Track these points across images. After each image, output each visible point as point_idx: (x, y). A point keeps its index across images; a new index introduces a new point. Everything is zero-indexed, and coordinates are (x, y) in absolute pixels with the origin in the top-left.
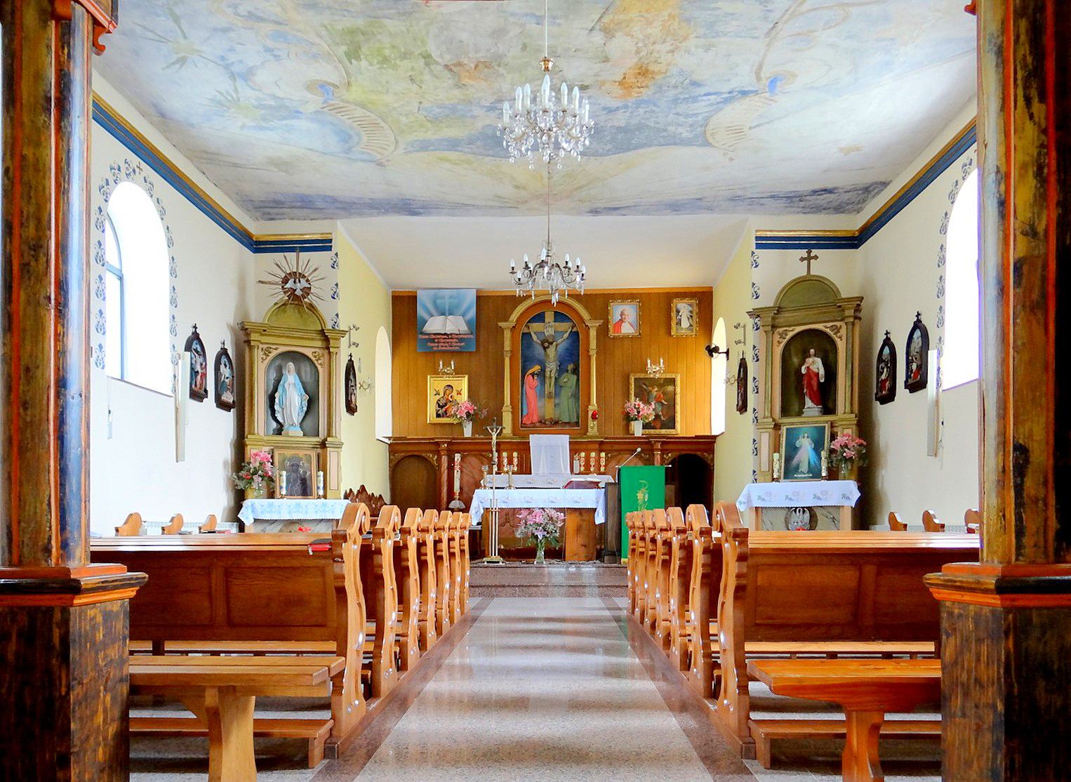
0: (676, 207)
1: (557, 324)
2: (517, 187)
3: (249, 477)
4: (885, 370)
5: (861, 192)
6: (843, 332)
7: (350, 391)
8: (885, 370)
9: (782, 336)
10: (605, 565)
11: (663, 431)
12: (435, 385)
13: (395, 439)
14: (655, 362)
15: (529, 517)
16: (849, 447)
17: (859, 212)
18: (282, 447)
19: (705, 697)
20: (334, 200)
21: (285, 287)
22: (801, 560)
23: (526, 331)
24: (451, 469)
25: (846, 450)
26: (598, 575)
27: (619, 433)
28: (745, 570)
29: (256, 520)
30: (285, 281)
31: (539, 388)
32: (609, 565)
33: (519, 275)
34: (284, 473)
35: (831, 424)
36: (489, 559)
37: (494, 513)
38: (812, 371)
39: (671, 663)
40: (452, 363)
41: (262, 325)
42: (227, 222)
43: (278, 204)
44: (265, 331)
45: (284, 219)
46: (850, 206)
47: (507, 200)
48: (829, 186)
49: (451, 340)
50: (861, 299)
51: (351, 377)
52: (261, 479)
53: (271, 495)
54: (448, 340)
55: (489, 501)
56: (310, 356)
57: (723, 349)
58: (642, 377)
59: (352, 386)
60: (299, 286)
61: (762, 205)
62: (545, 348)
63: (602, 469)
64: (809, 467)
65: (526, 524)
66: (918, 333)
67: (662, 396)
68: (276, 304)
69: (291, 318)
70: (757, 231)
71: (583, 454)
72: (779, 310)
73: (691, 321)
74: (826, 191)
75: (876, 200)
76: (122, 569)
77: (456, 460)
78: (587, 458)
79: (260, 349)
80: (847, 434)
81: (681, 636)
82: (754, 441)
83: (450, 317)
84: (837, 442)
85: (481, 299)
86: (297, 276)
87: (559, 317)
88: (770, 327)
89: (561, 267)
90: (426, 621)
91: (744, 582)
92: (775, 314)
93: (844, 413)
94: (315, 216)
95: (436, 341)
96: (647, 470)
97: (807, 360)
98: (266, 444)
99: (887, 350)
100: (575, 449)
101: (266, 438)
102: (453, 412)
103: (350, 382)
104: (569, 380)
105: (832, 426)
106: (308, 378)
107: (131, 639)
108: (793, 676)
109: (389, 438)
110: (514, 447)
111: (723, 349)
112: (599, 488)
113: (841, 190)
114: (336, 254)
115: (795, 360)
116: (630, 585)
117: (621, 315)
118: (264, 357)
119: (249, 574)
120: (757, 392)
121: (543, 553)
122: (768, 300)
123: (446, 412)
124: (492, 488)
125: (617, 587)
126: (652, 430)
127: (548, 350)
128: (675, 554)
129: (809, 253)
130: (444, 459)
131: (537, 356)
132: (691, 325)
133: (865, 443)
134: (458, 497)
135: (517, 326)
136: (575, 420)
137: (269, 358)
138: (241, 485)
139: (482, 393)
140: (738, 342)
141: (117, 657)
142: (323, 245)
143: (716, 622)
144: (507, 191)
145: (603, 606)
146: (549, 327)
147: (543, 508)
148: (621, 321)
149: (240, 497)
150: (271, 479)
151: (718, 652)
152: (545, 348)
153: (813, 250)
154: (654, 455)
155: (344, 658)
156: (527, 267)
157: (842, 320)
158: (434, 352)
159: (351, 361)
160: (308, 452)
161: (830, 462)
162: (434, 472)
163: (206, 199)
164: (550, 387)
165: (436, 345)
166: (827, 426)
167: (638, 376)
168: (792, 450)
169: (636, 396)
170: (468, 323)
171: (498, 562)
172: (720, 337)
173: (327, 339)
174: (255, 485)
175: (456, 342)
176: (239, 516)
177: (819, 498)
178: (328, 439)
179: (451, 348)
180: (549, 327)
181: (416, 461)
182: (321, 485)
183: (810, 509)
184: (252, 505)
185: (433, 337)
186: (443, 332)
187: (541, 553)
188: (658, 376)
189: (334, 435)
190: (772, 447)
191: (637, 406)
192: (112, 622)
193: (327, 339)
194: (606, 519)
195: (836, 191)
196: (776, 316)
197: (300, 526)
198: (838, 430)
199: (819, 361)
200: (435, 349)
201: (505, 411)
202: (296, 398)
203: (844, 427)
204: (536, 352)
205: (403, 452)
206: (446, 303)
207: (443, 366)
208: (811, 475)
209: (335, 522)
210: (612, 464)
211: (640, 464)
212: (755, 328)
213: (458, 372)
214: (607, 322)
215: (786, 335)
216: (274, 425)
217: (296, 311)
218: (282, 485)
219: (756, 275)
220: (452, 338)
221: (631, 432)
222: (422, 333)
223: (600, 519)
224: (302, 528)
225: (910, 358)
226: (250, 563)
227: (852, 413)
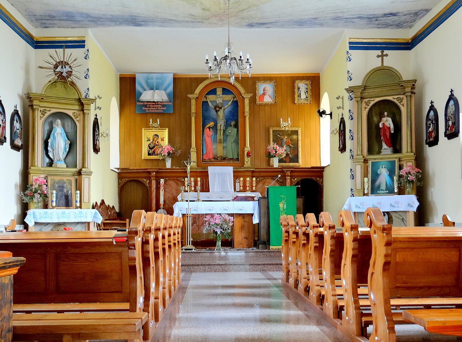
0: (301, 23)
1: (224, 96)
2: (204, 9)
3: (32, 194)
4: (431, 125)
5: (413, 15)
6: (404, 101)
7: (96, 138)
8: (431, 125)
9: (367, 104)
10: (260, 251)
11: (291, 164)
12: (147, 135)
13: (122, 169)
14: (285, 120)
15: (212, 220)
16: (411, 174)
17: (411, 28)
18: (53, 175)
19: (357, 336)
20: (88, 16)
21: (56, 71)
22: (424, 245)
23: (205, 100)
24: (158, 189)
25: (409, 175)
26: (247, 257)
27: (264, 165)
28: (390, 252)
29: (36, 223)
30: (56, 67)
31: (213, 136)
32: (263, 250)
33: (210, 65)
34: (54, 192)
35: (399, 159)
36: (186, 248)
37: (189, 217)
38: (386, 126)
39: (326, 315)
40: (158, 120)
41: (41, 95)
42: (19, 28)
43: (51, 17)
44: (42, 99)
45: (54, 27)
46: (406, 24)
47: (197, 17)
48: (394, 11)
49: (158, 106)
50: (415, 81)
51: (97, 129)
52: (39, 196)
53: (46, 206)
54: (155, 106)
55: (186, 209)
56: (71, 115)
57: (328, 112)
58: (277, 129)
59: (97, 135)
60: (65, 70)
61: (353, 22)
62: (217, 111)
63: (254, 188)
64: (386, 186)
65: (209, 225)
66: (452, 102)
67: (290, 141)
68: (50, 81)
69: (60, 91)
70: (350, 39)
71: (242, 179)
72: (365, 88)
73: (307, 95)
74: (392, 14)
75: (422, 19)
76: (10, 254)
77: (161, 183)
78: (245, 182)
79: (39, 111)
80: (409, 166)
81: (333, 296)
82: (351, 170)
83: (156, 91)
84: (404, 170)
85: (176, 80)
86: (63, 64)
87: (226, 91)
88: (360, 98)
89: (237, 60)
90: (165, 288)
91: (389, 259)
92: (362, 90)
93: (407, 152)
94: (75, 26)
95: (148, 106)
96: (283, 188)
97: (383, 119)
98: (42, 173)
99: (432, 113)
100: (237, 175)
101: (42, 169)
102: (159, 152)
103: (96, 132)
104: (232, 131)
105: (400, 161)
106: (69, 129)
107: (14, 303)
108: (438, 320)
109: (118, 169)
110: (198, 174)
111: (328, 112)
112: (254, 200)
113: (401, 14)
114: (88, 50)
115: (375, 119)
116: (284, 263)
117: (264, 90)
118: (42, 116)
119: (72, 258)
120: (352, 139)
121: (220, 243)
122: (358, 81)
123: (154, 152)
124: (187, 201)
125: (270, 264)
126: (284, 163)
127: (219, 113)
128: (326, 242)
129: (382, 52)
130: (154, 182)
131: (212, 116)
132: (307, 97)
133: (421, 171)
134: (162, 207)
135: (199, 97)
136: (236, 157)
137: (45, 117)
138: (26, 200)
139: (177, 139)
140: (339, 108)
141: (7, 315)
142: (80, 44)
143: (367, 286)
144: (197, 11)
145: (264, 277)
146: (219, 98)
147: (220, 214)
148: (264, 94)
149: (25, 208)
150: (46, 196)
151: (370, 306)
152: (217, 111)
153: (384, 51)
154: (286, 179)
155: (147, 313)
156: (216, 59)
157: (404, 94)
158: (147, 113)
159: (96, 119)
160: (70, 178)
161: (400, 183)
162: (147, 191)
163: (6, 13)
164: (220, 136)
165: (148, 108)
166: (397, 160)
167: (275, 129)
168: (375, 176)
169: (274, 141)
170: (168, 95)
171: (192, 249)
172: (325, 104)
173: (82, 105)
174: (35, 200)
175: (160, 107)
176: (25, 220)
177: (394, 206)
178: (83, 169)
179: (157, 111)
180: (219, 98)
181: (136, 184)
182: (78, 200)
183: (388, 213)
184: (33, 213)
185: (146, 104)
186: (152, 101)
187: (219, 243)
188: (287, 129)
189: (86, 167)
190: (363, 174)
191: (275, 148)
192: (4, 291)
193: (82, 105)
194: (260, 220)
195: (398, 15)
196: (363, 91)
197: (65, 227)
198: (404, 163)
199: (390, 120)
200: (147, 111)
201: (192, 152)
202: (62, 143)
203: (408, 161)
204: (212, 113)
205: (127, 178)
206: (154, 82)
207: (152, 123)
208: (388, 191)
209: (87, 224)
210: (260, 185)
211: (277, 185)
212: (350, 99)
213: (162, 126)
214: (255, 95)
215: (370, 103)
216: (47, 160)
217: (63, 86)
218: (77, 200)
219: (350, 66)
220: (158, 105)
221: (271, 165)
222: (138, 101)
223: (256, 220)
224: (66, 228)
225: (447, 118)
226: (73, 250)
227: (412, 152)
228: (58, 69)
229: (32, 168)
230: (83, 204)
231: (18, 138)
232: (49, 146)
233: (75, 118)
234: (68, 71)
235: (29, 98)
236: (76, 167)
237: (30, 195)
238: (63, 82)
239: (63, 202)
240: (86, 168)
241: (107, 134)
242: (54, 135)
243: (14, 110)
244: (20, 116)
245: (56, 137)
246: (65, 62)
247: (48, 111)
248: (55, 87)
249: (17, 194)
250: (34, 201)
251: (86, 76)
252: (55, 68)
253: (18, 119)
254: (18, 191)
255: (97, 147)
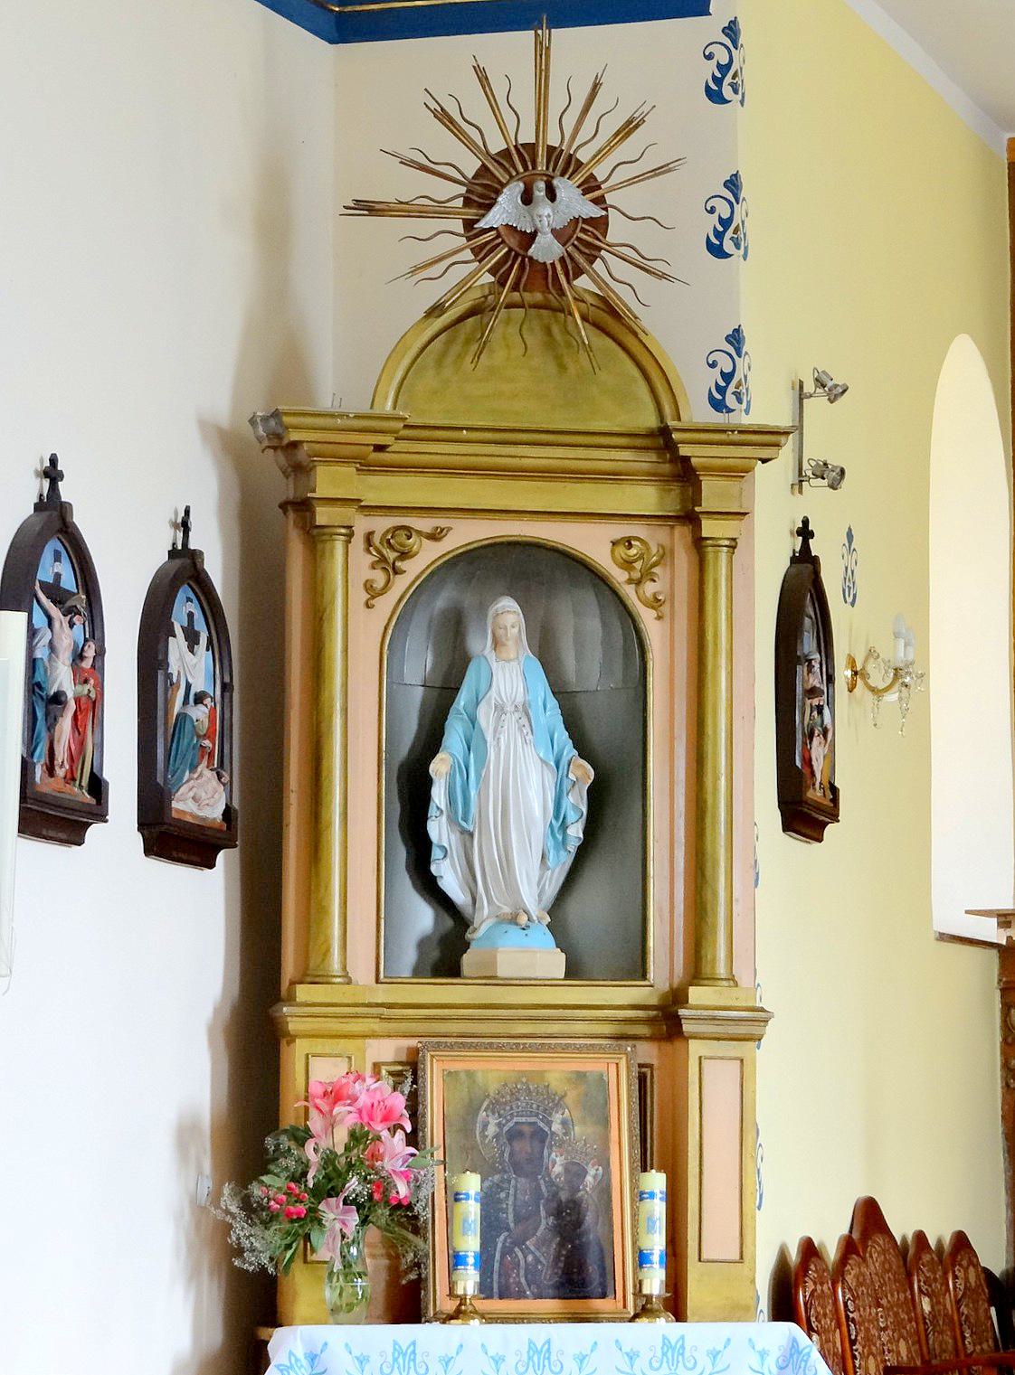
7: (802, 719)
21: (482, 224)
30: (482, 194)
34: (472, 1183)
41: (368, 422)
44: (380, 448)
52: (354, 1219)
60: (547, 216)
68: (436, 310)
79: (358, 541)
101: (383, 994)
114: (732, 30)
118: (379, 578)
137: (401, 584)
138: (261, 1246)
150: (408, 1219)
159: (805, 562)
160: (592, 1065)
173: (685, 475)
174: (326, 1248)
178: (692, 990)
182: (656, 1242)
184: (312, 1358)
189: (721, 970)
216: (423, 917)
217: (534, 339)
228: (495, 209)
229: (303, 993)
230: (695, 1274)
231: (202, 767)
232: (432, 811)
233: (630, 581)
234: (576, 221)
235: (282, 448)
236: (637, 969)
237: (289, 1214)
238: (535, 306)
239: (537, 1261)
240: (714, 979)
241: (896, 669)
242: (473, 721)
243: (173, 554)
244: (219, 595)
245: (489, 738)
246: (551, 149)
247: (425, 541)
248: (474, 347)
249: (194, 1201)
250: (314, 1257)
251: (719, 235)
252: (480, 206)
253: (198, 616)
254: (200, 1173)
255: (810, 794)
